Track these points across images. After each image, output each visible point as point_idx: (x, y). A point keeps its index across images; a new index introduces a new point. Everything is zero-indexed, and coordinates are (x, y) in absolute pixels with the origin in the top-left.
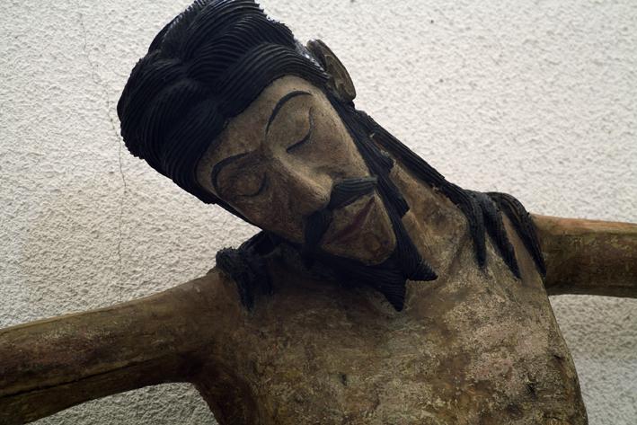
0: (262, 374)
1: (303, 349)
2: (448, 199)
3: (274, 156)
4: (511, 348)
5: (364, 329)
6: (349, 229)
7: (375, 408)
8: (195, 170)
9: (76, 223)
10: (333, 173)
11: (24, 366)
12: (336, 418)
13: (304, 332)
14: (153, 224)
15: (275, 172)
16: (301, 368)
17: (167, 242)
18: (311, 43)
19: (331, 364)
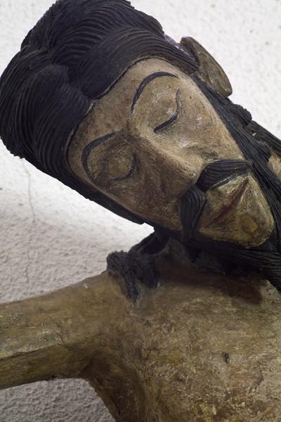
0: (147, 359)
1: (187, 333)
3: (141, 136)
5: (249, 313)
6: (226, 210)
7: (258, 384)
8: (67, 156)
10: (203, 153)
12: (218, 394)
13: (189, 318)
14: (61, 250)
15: (144, 152)
16: (184, 350)
17: (74, 265)
18: (184, 40)
19: (214, 345)
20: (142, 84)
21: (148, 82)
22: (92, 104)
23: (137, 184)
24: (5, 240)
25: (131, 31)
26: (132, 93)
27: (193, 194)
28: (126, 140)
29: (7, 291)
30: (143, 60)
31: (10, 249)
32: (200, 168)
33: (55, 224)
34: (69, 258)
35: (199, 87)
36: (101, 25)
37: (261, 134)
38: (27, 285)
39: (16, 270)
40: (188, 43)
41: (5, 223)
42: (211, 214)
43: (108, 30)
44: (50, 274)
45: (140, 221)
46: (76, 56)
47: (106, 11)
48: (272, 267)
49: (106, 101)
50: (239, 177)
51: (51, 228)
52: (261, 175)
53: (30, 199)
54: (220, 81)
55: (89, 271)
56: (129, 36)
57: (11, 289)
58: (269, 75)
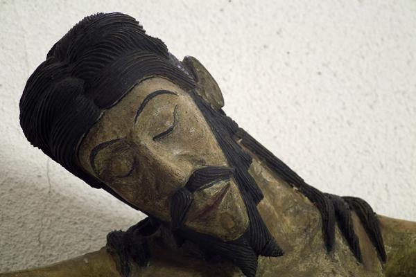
2: (306, 198)
3: (142, 143)
6: (209, 209)
9: (4, 214)
10: (193, 160)
14: (70, 219)
18: (186, 59)
20: (145, 99)
21: (151, 98)
22: (102, 113)
23: (135, 181)
24: (22, 207)
25: (140, 54)
26: (137, 107)
27: (182, 194)
28: (128, 146)
29: (21, 253)
30: (148, 79)
31: (26, 215)
32: (189, 174)
33: (68, 195)
34: (77, 226)
35: (195, 102)
36: (114, 48)
37: (247, 140)
38: (38, 248)
39: (30, 234)
40: (190, 62)
41: (24, 192)
42: (196, 211)
43: (119, 51)
44: (59, 240)
46: (91, 72)
47: (120, 36)
48: (244, 259)
49: (114, 111)
50: (222, 182)
51: (64, 198)
52: (241, 180)
53: (48, 172)
54: (215, 95)
55: (93, 238)
56: (138, 58)
57: (24, 251)
58: (264, 75)
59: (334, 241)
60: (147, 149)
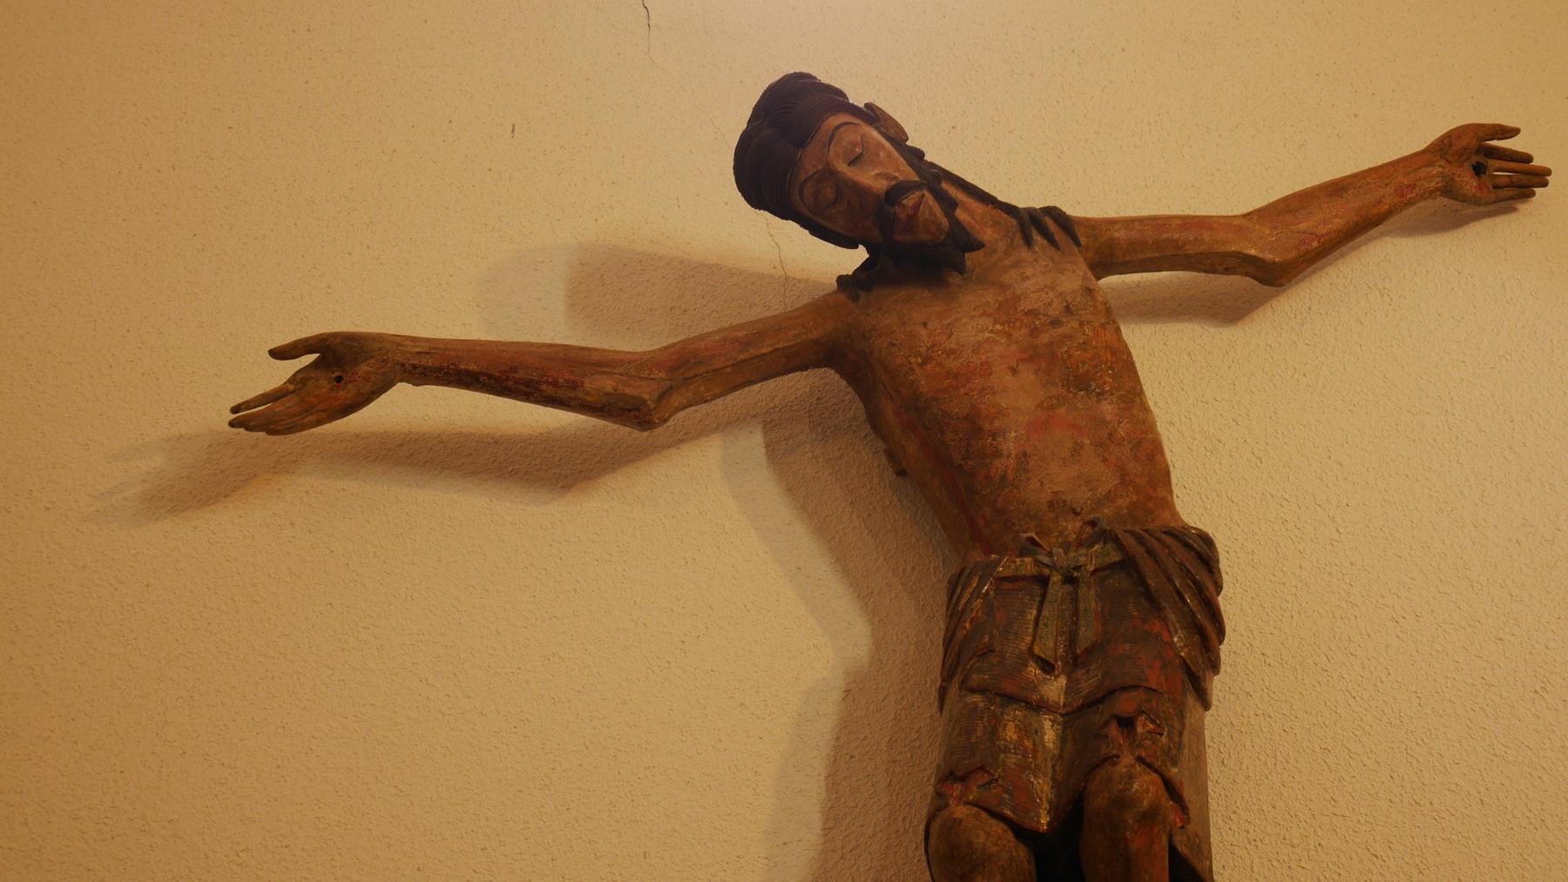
3: (839, 169)
4: (1052, 288)
6: (911, 218)
11: (695, 358)
40: (868, 106)
45: (851, 244)
50: (917, 193)
51: (800, 281)
58: (957, 150)
59: (1032, 238)
60: (844, 173)
